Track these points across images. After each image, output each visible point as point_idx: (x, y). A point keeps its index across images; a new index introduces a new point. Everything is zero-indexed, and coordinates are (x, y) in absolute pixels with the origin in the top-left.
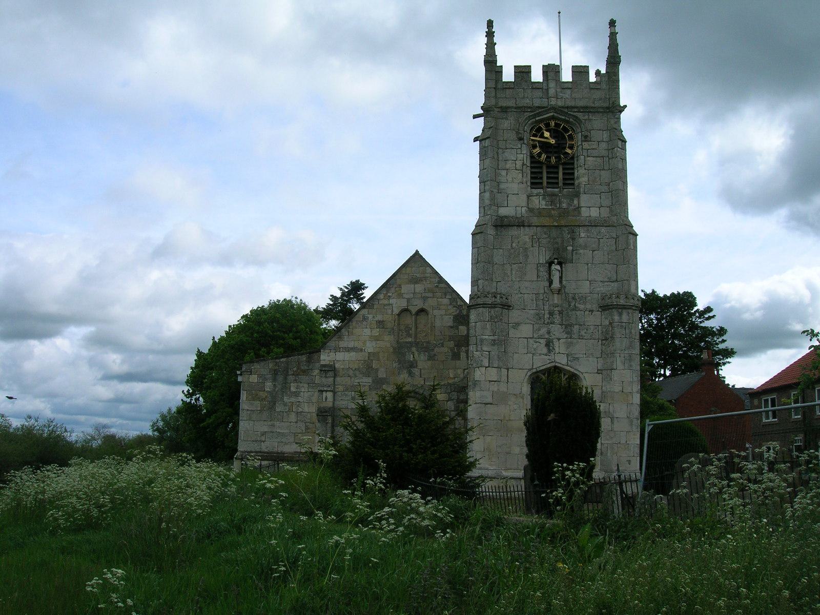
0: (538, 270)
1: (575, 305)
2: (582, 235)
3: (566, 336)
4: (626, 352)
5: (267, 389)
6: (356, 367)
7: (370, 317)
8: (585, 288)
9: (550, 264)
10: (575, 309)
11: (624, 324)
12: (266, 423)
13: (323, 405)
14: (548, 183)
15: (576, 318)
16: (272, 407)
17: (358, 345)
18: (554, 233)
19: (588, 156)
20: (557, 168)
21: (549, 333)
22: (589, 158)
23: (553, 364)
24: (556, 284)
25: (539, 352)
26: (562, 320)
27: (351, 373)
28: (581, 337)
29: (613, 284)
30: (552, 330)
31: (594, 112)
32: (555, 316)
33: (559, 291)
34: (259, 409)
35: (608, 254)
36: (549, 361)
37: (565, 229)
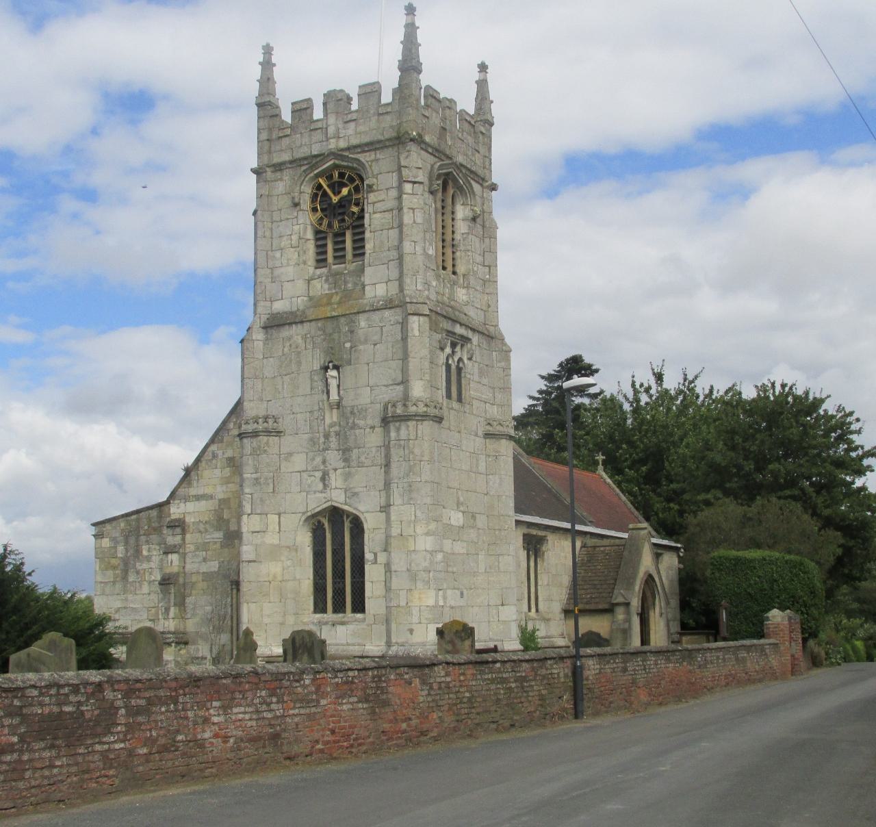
0: (312, 380)
1: (354, 421)
2: (363, 324)
3: (343, 464)
4: (405, 480)
5: (120, 555)
6: (207, 519)
7: (220, 453)
8: (365, 397)
9: (326, 369)
10: (354, 426)
11: (402, 442)
12: (119, 597)
13: (168, 571)
14: (335, 257)
15: (356, 440)
16: (125, 577)
17: (209, 490)
18: (330, 326)
19: (374, 213)
20: (344, 234)
21: (324, 462)
22: (375, 216)
23: (329, 504)
24: (334, 396)
25: (314, 489)
26: (339, 444)
27: (201, 527)
28: (361, 465)
29: (398, 387)
30: (328, 458)
31: (382, 148)
32: (331, 439)
33: (338, 405)
34: (112, 580)
35: (392, 347)
36: (324, 501)
37: (342, 320)
